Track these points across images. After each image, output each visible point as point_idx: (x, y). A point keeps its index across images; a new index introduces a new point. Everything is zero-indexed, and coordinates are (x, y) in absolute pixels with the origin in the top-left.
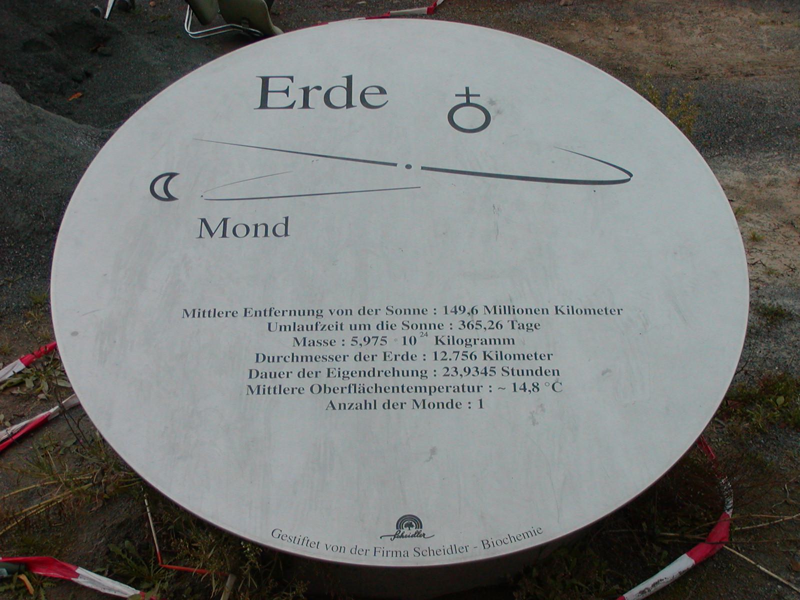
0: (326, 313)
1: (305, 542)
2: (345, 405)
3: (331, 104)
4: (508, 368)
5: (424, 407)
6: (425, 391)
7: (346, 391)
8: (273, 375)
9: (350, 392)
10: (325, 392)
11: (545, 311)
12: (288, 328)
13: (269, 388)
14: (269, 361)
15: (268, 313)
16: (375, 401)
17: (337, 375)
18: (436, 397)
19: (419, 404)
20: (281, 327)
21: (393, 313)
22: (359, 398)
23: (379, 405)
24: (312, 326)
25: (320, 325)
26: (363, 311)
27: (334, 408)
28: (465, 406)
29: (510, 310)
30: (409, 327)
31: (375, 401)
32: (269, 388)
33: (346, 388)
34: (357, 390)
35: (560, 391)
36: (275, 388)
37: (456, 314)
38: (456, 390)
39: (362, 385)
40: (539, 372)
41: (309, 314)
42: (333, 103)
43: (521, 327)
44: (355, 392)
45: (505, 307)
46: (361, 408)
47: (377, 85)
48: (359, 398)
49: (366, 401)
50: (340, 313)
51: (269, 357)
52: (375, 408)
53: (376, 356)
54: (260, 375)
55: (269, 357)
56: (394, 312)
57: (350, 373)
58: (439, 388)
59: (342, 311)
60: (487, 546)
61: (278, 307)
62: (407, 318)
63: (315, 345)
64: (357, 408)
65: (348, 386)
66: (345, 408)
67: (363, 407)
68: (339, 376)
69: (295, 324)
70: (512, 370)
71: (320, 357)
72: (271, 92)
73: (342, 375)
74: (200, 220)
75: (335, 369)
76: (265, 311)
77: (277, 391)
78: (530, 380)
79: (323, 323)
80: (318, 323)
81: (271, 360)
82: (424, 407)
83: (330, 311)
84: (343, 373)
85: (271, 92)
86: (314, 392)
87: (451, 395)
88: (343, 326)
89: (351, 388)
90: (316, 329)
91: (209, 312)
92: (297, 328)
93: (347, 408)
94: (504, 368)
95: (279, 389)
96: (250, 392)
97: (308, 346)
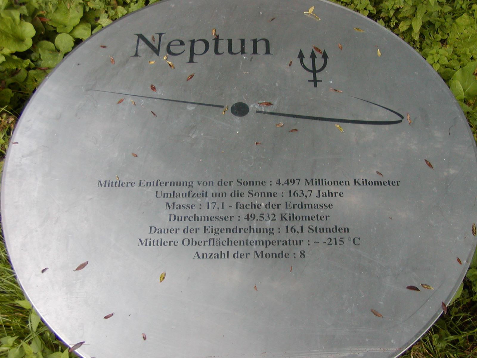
0: (195, 184)
2: (206, 254)
4: (313, 226)
5: (262, 257)
6: (263, 244)
7: (207, 243)
8: (166, 231)
9: (210, 244)
10: (192, 244)
11: (347, 183)
12: (169, 195)
13: (154, 241)
14: (178, 220)
16: (228, 252)
17: (211, 232)
19: (259, 255)
21: (241, 184)
23: (231, 255)
24: (186, 194)
25: (191, 193)
26: (221, 183)
27: (199, 257)
28: (291, 255)
29: (321, 182)
31: (228, 252)
32: (154, 241)
33: (207, 241)
34: (215, 243)
35: (359, 244)
36: (158, 241)
37: (288, 185)
38: (285, 244)
39: (218, 239)
40: (334, 230)
41: (256, 184)
42: (203, 42)
43: (324, 195)
44: (213, 245)
45: (319, 180)
46: (218, 257)
51: (178, 217)
52: (228, 257)
54: (157, 231)
55: (178, 217)
56: (242, 184)
57: (220, 230)
58: (272, 242)
59: (372, 182)
62: (251, 188)
63: (181, 208)
64: (215, 257)
65: (208, 240)
66: (206, 257)
67: (219, 256)
68: (212, 232)
69: (174, 192)
70: (316, 228)
71: (214, 217)
72: (221, 39)
74: (137, 37)
75: (209, 227)
76: (154, 182)
78: (338, 235)
79: (194, 192)
80: (190, 192)
81: (180, 219)
82: (262, 257)
83: (198, 182)
84: (215, 230)
85: (221, 39)
86: (185, 244)
88: (207, 194)
89: (211, 242)
90: (189, 196)
93: (208, 257)
94: (310, 227)
95: (160, 241)
96: (140, 244)
97: (176, 209)
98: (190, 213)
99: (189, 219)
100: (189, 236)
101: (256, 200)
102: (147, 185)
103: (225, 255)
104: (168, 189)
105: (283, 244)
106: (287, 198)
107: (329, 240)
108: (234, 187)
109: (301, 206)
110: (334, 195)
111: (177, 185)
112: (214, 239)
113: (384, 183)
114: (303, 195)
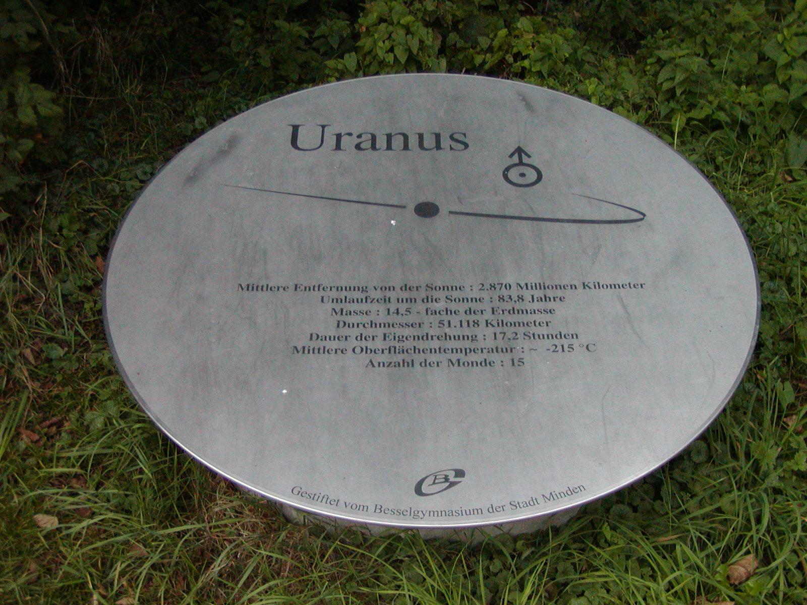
1: (325, 500)
2: (384, 363)
3: (297, 146)
12: (339, 301)
13: (314, 349)
15: (316, 289)
16: (413, 361)
18: (473, 357)
20: (333, 300)
22: (399, 358)
27: (373, 366)
30: (452, 301)
34: (397, 351)
47: (301, 152)
48: (399, 358)
49: (403, 360)
50: (384, 289)
53: (423, 323)
54: (320, 338)
57: (405, 337)
60: (378, 511)
61: (326, 283)
64: (395, 366)
65: (388, 348)
68: (395, 339)
69: (346, 297)
73: (397, 339)
76: (314, 287)
77: (321, 351)
84: (399, 337)
87: (485, 355)
90: (366, 302)
91: (262, 287)
92: (348, 300)
98: (365, 319)
99: (364, 326)
100: (364, 344)
101: (453, 306)
102: (305, 290)
103: (408, 363)
104: (334, 294)
105: (489, 352)
106: (496, 303)
107: (554, 347)
108: (423, 294)
109: (513, 311)
110: (552, 299)
111: (262, 290)
112: (395, 348)
113: (623, 285)
114: (511, 300)
